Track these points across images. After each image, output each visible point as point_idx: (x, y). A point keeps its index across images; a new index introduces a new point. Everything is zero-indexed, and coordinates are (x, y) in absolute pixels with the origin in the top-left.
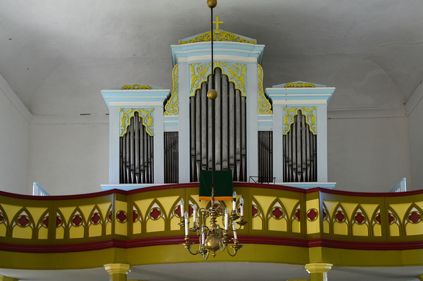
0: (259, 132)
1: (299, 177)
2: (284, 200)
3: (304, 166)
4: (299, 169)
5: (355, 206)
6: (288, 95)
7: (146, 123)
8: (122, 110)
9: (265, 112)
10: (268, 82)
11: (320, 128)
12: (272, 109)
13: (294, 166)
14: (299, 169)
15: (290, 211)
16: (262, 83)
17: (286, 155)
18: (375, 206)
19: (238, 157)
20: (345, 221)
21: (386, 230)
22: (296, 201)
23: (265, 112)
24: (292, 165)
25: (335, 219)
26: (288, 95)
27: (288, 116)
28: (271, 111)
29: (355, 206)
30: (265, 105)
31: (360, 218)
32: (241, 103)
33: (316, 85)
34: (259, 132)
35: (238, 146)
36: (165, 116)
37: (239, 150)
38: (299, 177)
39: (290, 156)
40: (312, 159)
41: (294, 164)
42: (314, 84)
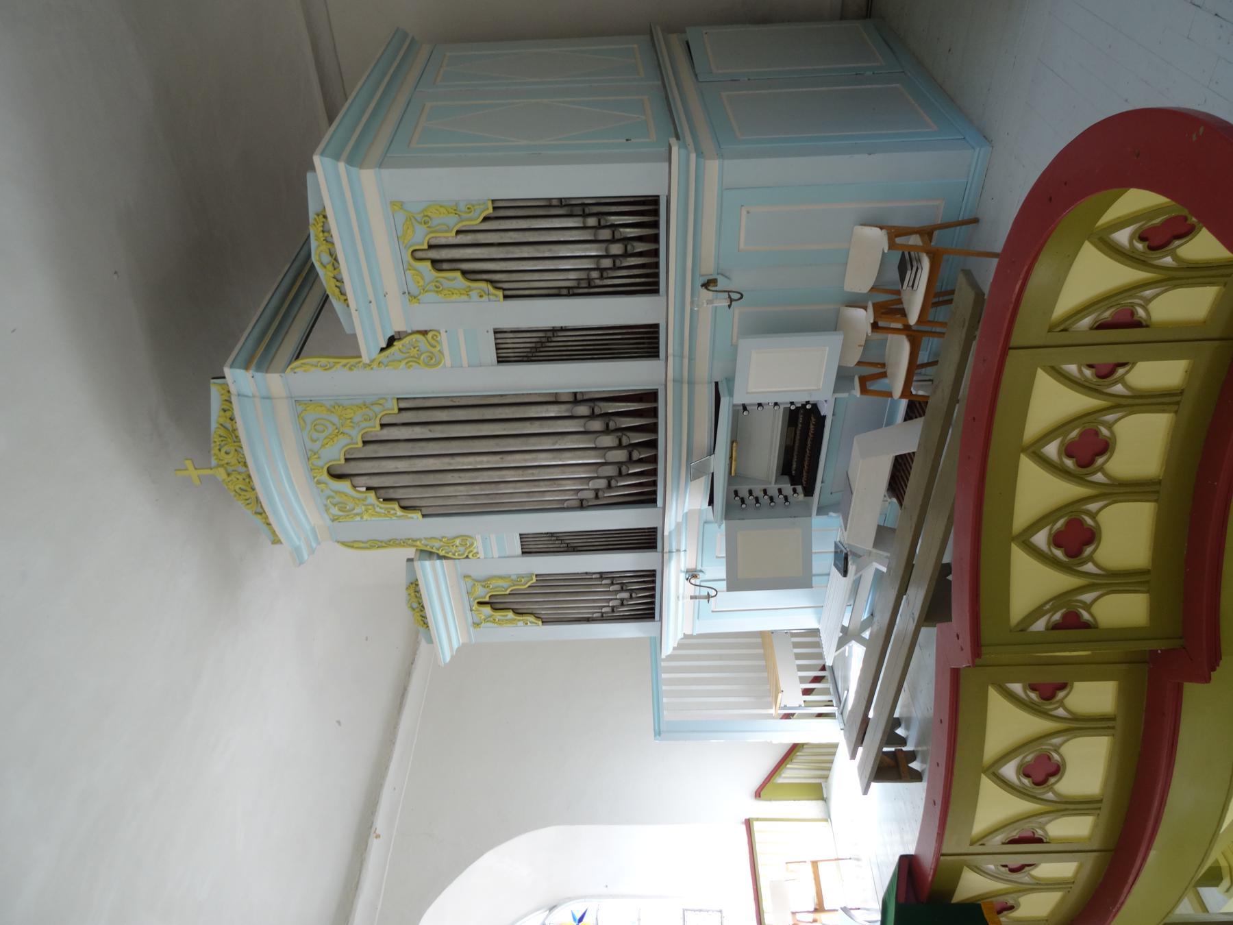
0: (501, 360)
1: (640, 247)
2: (994, 745)
3: (605, 234)
4: (616, 249)
5: (1028, 468)
6: (371, 297)
7: (504, 587)
8: (476, 624)
9: (435, 350)
10: (346, 347)
11: (464, 187)
12: (425, 333)
13: (606, 263)
14: (616, 249)
15: (1033, 725)
16: (344, 361)
17: (568, 288)
18: (1044, 382)
19: (583, 410)
20: (1093, 516)
21: (1171, 340)
22: (994, 696)
23: (435, 350)
24: (602, 270)
25: (1084, 562)
26: (371, 297)
27: (438, 289)
28: (430, 335)
29: (1028, 468)
30: (414, 352)
31: (1086, 448)
32: (418, 412)
33: (312, 209)
34: (501, 360)
35: (552, 411)
36: (481, 555)
37: (564, 407)
38: (640, 247)
39: (572, 275)
40: (578, 210)
41: (598, 263)
42: (312, 215)
